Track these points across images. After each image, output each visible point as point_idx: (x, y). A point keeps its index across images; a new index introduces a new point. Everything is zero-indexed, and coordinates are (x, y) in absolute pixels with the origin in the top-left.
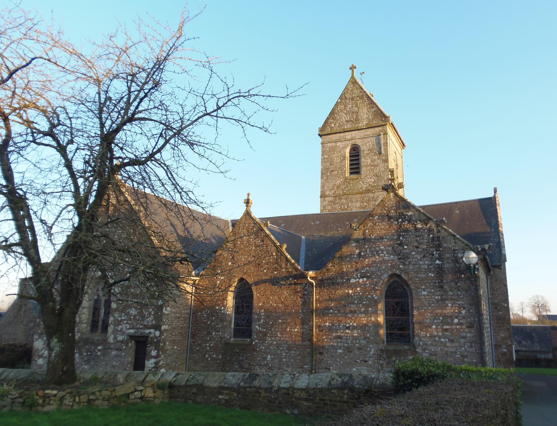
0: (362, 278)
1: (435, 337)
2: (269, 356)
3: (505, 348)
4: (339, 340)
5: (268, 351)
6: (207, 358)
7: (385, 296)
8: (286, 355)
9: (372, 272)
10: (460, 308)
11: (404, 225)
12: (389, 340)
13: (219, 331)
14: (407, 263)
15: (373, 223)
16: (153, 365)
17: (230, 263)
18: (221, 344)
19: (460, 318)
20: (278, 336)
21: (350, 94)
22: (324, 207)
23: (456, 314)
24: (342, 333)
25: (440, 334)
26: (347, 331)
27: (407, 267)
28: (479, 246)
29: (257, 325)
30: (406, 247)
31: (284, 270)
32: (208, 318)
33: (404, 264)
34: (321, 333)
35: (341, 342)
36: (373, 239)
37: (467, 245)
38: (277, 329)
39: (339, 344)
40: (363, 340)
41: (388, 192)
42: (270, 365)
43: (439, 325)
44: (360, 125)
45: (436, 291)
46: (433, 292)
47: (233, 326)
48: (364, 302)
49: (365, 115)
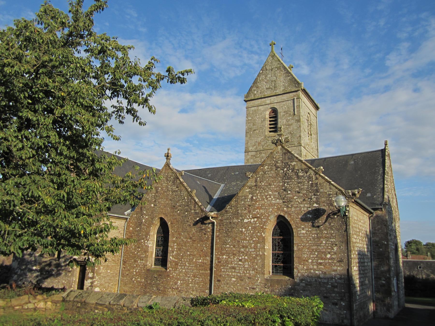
0: (253, 218)
1: (311, 269)
2: (179, 282)
3: (384, 280)
4: (234, 270)
5: (178, 277)
6: (134, 281)
7: (273, 234)
8: (192, 281)
9: (261, 213)
10: (332, 245)
11: (288, 173)
12: (274, 271)
13: (143, 260)
14: (290, 206)
15: (263, 172)
16: (90, 284)
17: (152, 205)
18: (144, 270)
19: (333, 253)
20: (186, 266)
21: (270, 66)
22: (248, 160)
23: (329, 250)
24: (236, 264)
25: (315, 267)
26: (240, 263)
27: (290, 209)
28: (350, 191)
29: (171, 256)
30: (289, 192)
31: (193, 211)
32: (135, 249)
33: (288, 207)
34: (220, 264)
35: (235, 272)
36: (263, 186)
37: (340, 190)
38: (186, 260)
39: (233, 274)
40: (252, 270)
41: (276, 145)
42: (180, 288)
43: (314, 260)
44: (278, 91)
45: (313, 230)
46: (310, 231)
47: (154, 256)
48: (255, 239)
49: (282, 83)
